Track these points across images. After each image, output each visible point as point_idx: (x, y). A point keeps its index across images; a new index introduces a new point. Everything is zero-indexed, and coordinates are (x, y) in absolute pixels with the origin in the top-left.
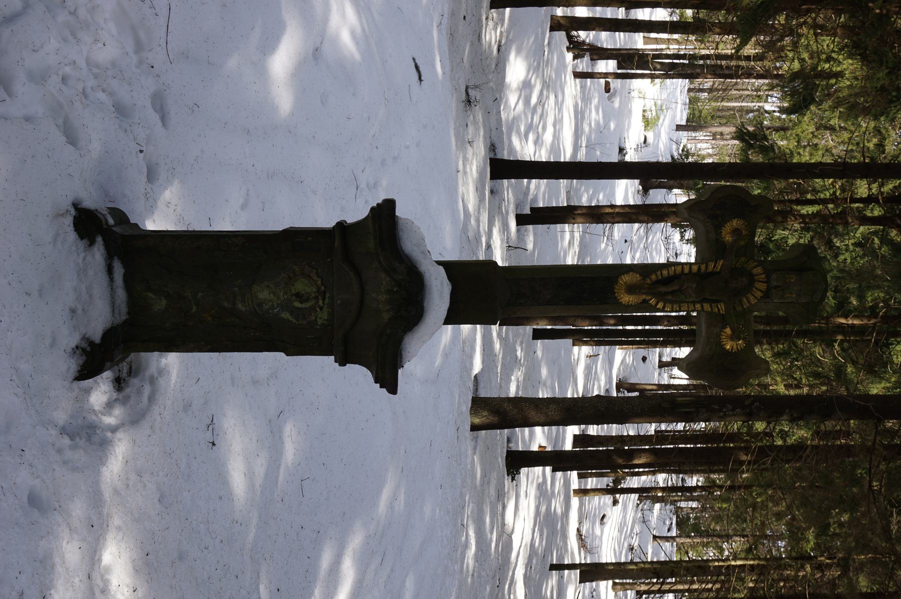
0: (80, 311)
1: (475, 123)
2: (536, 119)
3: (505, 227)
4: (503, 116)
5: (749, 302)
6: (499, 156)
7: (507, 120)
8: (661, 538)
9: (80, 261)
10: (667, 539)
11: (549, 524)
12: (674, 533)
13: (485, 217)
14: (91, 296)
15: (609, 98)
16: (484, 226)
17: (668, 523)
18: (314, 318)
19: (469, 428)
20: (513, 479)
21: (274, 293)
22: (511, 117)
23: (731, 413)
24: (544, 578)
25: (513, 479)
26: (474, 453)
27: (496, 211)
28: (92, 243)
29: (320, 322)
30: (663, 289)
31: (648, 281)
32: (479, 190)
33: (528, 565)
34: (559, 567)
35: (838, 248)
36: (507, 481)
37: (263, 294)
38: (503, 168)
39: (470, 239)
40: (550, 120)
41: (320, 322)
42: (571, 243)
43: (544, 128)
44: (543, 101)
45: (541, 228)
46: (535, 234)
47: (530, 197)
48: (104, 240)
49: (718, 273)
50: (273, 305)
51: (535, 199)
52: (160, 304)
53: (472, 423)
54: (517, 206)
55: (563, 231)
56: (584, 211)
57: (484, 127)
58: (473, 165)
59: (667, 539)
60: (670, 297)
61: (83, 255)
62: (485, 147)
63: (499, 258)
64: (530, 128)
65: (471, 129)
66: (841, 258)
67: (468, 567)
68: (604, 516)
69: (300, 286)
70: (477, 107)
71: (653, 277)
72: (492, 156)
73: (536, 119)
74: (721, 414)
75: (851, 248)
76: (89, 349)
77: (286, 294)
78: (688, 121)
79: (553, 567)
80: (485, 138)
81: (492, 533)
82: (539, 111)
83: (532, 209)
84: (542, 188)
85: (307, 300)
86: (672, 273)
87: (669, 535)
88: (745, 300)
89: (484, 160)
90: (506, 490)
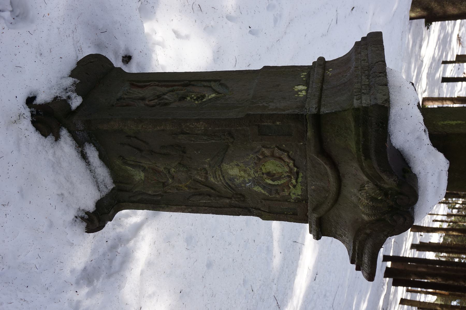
0: (66, 194)
9: (51, 157)
11: (444, 42)
14: (72, 183)
18: (287, 194)
20: (428, 28)
21: (245, 171)
24: (437, 69)
25: (428, 28)
28: (57, 138)
29: (293, 197)
34: (445, 62)
37: (234, 171)
41: (293, 197)
48: (70, 131)
50: (245, 181)
52: (139, 176)
53: (410, 16)
61: (51, 151)
69: (271, 166)
76: (86, 216)
77: (257, 172)
81: (414, 72)
85: (279, 178)
90: (424, 36)
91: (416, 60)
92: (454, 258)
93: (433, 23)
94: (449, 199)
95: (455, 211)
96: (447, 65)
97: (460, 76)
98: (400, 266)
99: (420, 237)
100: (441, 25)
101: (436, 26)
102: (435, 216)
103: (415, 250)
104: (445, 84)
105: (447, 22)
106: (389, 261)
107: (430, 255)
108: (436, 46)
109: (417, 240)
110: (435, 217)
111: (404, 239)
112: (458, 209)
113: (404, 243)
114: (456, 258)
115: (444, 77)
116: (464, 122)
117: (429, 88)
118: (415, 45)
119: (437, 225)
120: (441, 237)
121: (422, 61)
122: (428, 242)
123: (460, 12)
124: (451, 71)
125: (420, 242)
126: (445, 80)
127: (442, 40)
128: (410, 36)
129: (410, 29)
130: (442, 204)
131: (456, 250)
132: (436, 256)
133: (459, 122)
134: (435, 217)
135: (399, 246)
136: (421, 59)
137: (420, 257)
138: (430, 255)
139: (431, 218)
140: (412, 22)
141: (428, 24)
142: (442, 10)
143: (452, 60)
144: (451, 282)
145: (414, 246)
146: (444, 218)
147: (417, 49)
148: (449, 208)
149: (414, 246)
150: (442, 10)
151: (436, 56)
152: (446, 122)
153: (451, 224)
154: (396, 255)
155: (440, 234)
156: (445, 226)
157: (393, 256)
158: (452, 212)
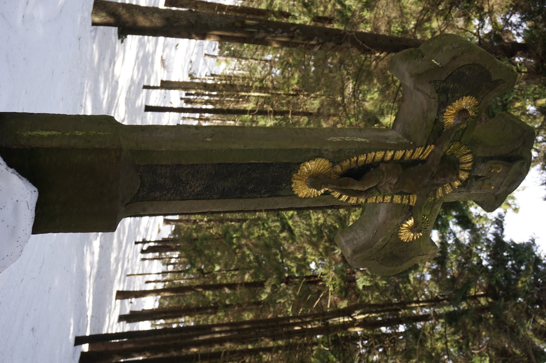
8: (209, 55)
11: (144, 62)
12: (216, 53)
17: (214, 46)
19: (91, 24)
20: (122, 42)
23: (280, 35)
24: (138, 95)
25: (122, 42)
26: (94, 42)
33: (129, 91)
49: (424, 162)
68: (177, 45)
74: (274, 35)
79: (145, 87)
81: (104, 94)
87: (213, 54)
88: (440, 190)
91: (106, 80)
92: (171, 324)
93: (129, 37)
94: (163, 254)
95: (170, 268)
96: (151, 90)
97: (166, 106)
98: (100, 347)
99: (130, 304)
100: (140, 41)
101: (132, 40)
102: (148, 276)
103: (125, 322)
104: (149, 114)
105: (146, 37)
106: (85, 343)
107: (145, 326)
108: (135, 66)
109: (126, 309)
110: (148, 278)
111: (107, 310)
112: (174, 264)
113: (108, 315)
114: (174, 323)
115: (148, 105)
116: (60, 133)
117: (128, 117)
118: (104, 59)
119: (150, 287)
120: (156, 301)
121: (117, 82)
122: (140, 309)
123: (152, 25)
124: (156, 98)
125: (131, 312)
126: (148, 109)
127: (142, 60)
128: (95, 46)
129: (94, 38)
130: (156, 261)
131: (170, 315)
132: (152, 325)
133: (54, 133)
134: (148, 278)
135: (99, 321)
136: (115, 79)
137: (132, 330)
138: (145, 326)
139: (143, 279)
140: (96, 29)
141: (122, 34)
142: (131, 19)
143: (155, 85)
144: (160, 355)
145: (122, 318)
146: (160, 277)
147: (106, 64)
148: (163, 265)
149: (122, 318)
150: (131, 19)
151: (135, 78)
152: (34, 133)
153: (167, 283)
154: (95, 333)
155: (155, 298)
156: (160, 286)
157: (91, 336)
158: (167, 269)
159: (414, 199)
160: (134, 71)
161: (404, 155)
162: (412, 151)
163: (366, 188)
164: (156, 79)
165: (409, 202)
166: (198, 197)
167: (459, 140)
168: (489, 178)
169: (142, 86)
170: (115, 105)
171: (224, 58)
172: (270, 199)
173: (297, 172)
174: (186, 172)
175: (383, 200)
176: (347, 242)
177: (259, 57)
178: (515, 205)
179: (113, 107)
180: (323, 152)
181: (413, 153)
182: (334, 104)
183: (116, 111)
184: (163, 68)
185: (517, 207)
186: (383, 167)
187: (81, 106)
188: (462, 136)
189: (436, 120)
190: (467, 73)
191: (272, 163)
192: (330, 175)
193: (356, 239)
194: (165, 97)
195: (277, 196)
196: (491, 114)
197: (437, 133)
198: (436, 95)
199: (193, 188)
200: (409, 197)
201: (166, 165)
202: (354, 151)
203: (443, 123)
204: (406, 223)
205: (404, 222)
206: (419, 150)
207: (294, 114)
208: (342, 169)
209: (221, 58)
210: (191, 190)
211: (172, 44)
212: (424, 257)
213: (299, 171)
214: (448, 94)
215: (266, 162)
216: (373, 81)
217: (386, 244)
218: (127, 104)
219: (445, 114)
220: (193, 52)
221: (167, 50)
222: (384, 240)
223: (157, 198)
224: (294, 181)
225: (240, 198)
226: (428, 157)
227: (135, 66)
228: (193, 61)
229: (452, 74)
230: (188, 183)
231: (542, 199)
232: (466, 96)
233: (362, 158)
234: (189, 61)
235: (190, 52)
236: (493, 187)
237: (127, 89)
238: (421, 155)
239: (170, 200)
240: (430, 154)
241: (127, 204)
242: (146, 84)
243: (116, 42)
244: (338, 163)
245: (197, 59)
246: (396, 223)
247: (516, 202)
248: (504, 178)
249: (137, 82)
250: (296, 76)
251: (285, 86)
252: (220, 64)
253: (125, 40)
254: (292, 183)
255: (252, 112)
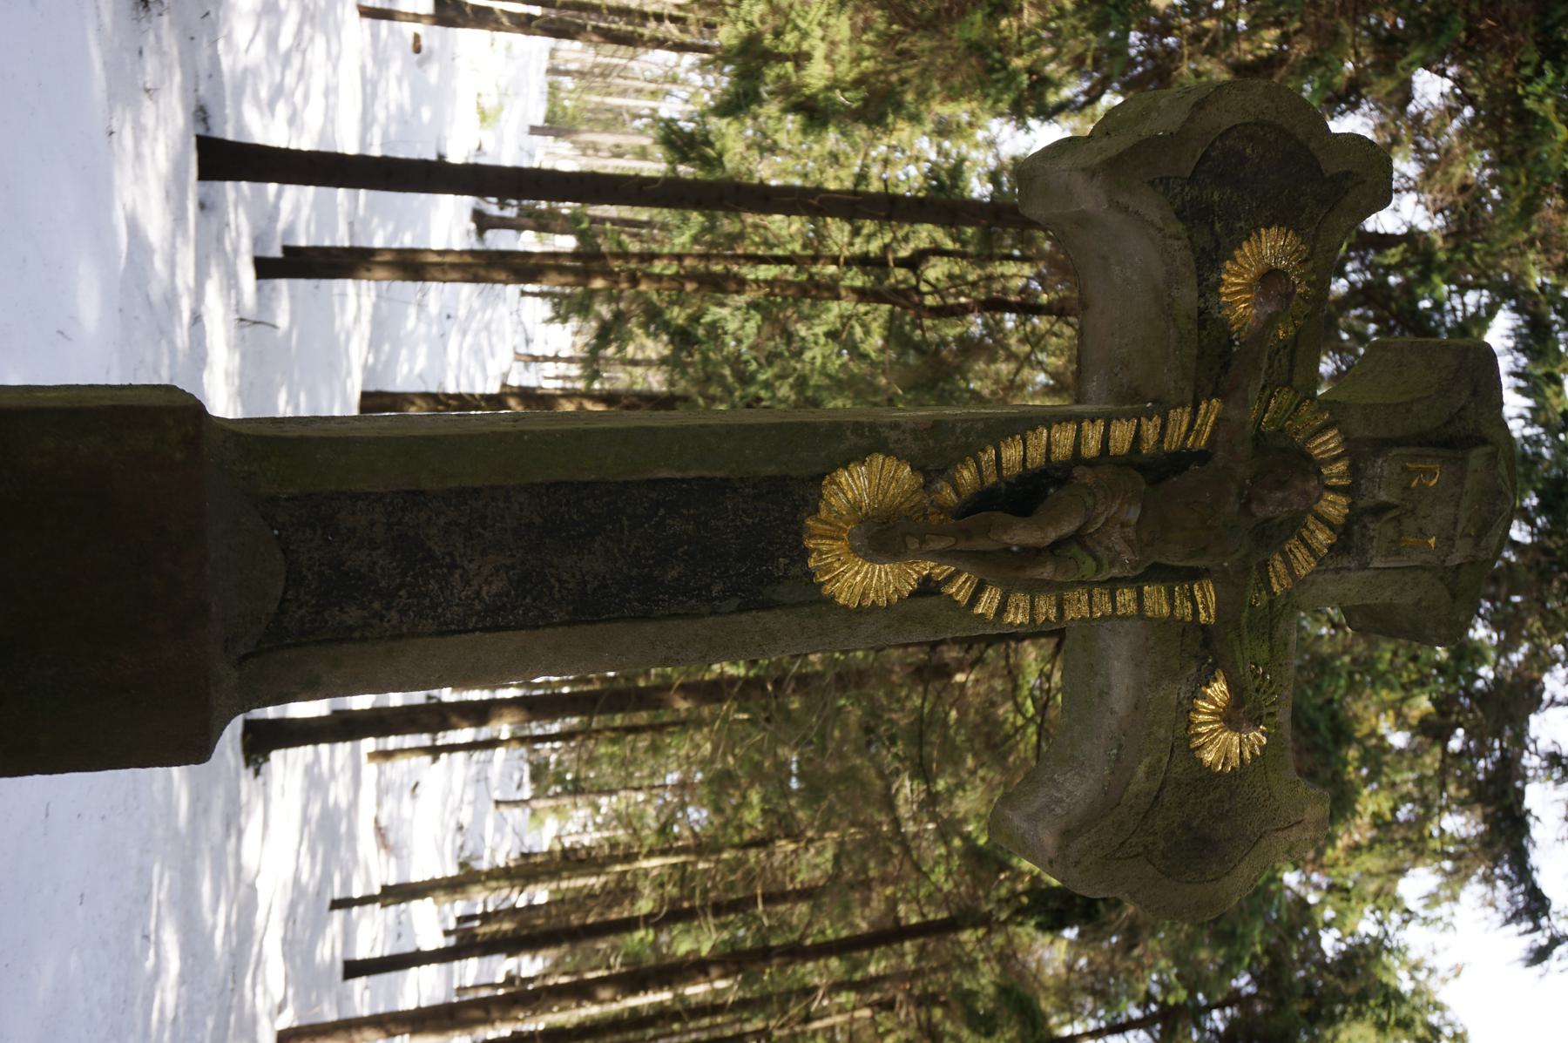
1: (160, 52)
2: (290, 78)
3: (231, 281)
4: (226, 63)
5: (1291, 571)
6: (216, 133)
7: (233, 71)
8: (507, 803)
10: (516, 803)
11: (327, 832)
12: (526, 793)
13: (187, 258)
15: (420, 64)
16: (186, 276)
17: (516, 776)
20: (257, 773)
22: (240, 66)
24: (318, 928)
25: (257, 773)
27: (211, 249)
30: (1021, 535)
31: (948, 495)
32: (175, 196)
33: (291, 917)
35: (803, 339)
36: (246, 775)
38: (224, 160)
39: (141, 301)
40: (317, 86)
42: (357, 320)
43: (306, 97)
44: (304, 45)
45: (302, 283)
46: (292, 297)
47: (281, 226)
49: (1203, 457)
51: (290, 230)
54: (257, 241)
55: (343, 295)
56: (387, 257)
57: (183, 65)
58: (159, 145)
59: (516, 803)
60: (1047, 572)
62: (186, 108)
63: (222, 403)
64: (278, 92)
65: (151, 63)
66: (807, 355)
67: (162, 1011)
70: (165, 19)
71: (967, 475)
72: (202, 132)
73: (290, 78)
75: (822, 340)
78: (546, 121)
79: (337, 904)
80: (184, 89)
81: (215, 911)
82: (296, 62)
83: (287, 250)
84: (305, 212)
86: (1036, 456)
87: (518, 797)
89: (185, 136)
96: (356, 910)
104: (359, 984)
108: (300, 844)
115: (351, 957)
117: (296, 995)
118: (206, 810)
121: (252, 888)
124: (373, 934)
126: (354, 969)
147: (217, 825)
151: (305, 877)
159: (1206, 600)
160: (302, 860)
161: (1137, 438)
162: (1157, 420)
163: (1052, 535)
164: (368, 882)
165: (1196, 612)
166: (495, 619)
167: (1289, 383)
168: (1413, 512)
169: (328, 903)
170: (253, 959)
171: (551, 803)
172: (744, 617)
173: (817, 510)
174: (442, 521)
175: (1114, 608)
176: (1033, 818)
177: (646, 783)
178: (1451, 1024)
179: (247, 965)
180: (886, 432)
181: (1164, 427)
182: (873, 842)
183: (259, 979)
184: (383, 851)
185: (1459, 1030)
186: (1085, 476)
187: (146, 937)
188: (1291, 371)
189: (1201, 312)
190: (1248, 151)
191: (728, 480)
192: (926, 516)
193: (1059, 801)
194: (399, 936)
195: (768, 606)
196: (1305, 725)
197: (1216, 360)
198: (1181, 226)
199: (475, 583)
200: (1191, 590)
201: (367, 494)
202: (980, 426)
203: (1224, 325)
204: (1205, 697)
205: (1196, 694)
206: (1180, 418)
207: (769, 899)
208: (958, 493)
209: (541, 804)
210: (469, 592)
211: (402, 785)
212: (1294, 834)
213: (822, 505)
214: (1213, 223)
215: (706, 474)
216: (964, 761)
217: (1161, 789)
218: (288, 956)
219: (1223, 290)
220: (462, 801)
221: (389, 803)
222: (1151, 772)
223: (351, 628)
224: (811, 544)
225: (646, 617)
226: (1212, 441)
227: (300, 844)
228: (466, 825)
229: (1205, 156)
230: (453, 566)
231: (1521, 964)
232: (1268, 228)
233: (1012, 453)
234: (453, 825)
235: (454, 800)
236: (1432, 541)
237: (284, 914)
238: (1187, 437)
239: (401, 636)
240: (1213, 432)
241: (244, 658)
242: (337, 895)
243: (238, 775)
244: (941, 472)
245: (475, 815)
246: (1173, 700)
247: (1449, 1015)
248: (1457, 505)
249: (311, 889)
250: (755, 797)
251: (730, 830)
252: (542, 823)
253: (264, 768)
254: (806, 553)
255: (649, 920)
